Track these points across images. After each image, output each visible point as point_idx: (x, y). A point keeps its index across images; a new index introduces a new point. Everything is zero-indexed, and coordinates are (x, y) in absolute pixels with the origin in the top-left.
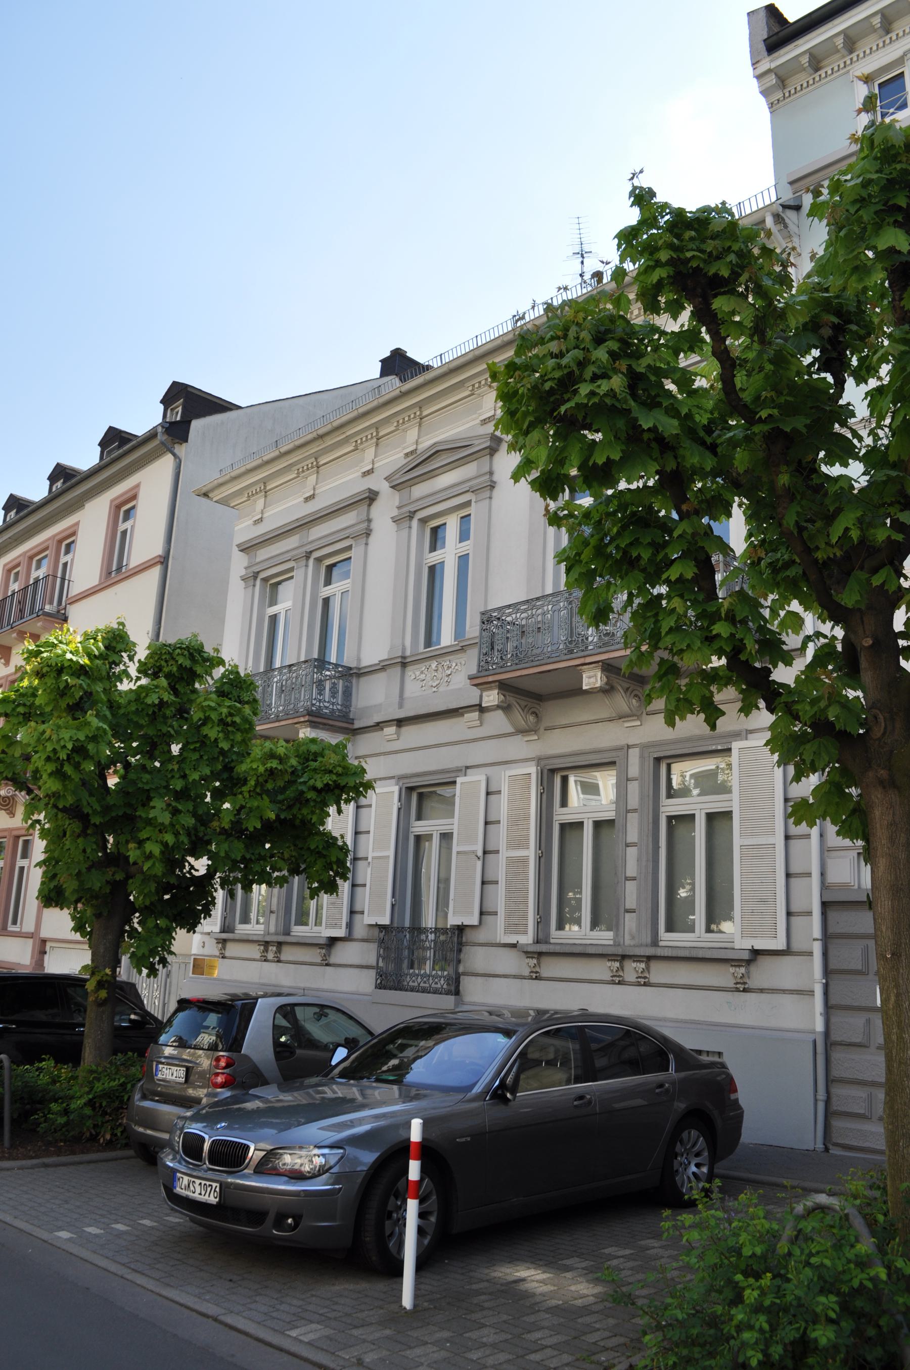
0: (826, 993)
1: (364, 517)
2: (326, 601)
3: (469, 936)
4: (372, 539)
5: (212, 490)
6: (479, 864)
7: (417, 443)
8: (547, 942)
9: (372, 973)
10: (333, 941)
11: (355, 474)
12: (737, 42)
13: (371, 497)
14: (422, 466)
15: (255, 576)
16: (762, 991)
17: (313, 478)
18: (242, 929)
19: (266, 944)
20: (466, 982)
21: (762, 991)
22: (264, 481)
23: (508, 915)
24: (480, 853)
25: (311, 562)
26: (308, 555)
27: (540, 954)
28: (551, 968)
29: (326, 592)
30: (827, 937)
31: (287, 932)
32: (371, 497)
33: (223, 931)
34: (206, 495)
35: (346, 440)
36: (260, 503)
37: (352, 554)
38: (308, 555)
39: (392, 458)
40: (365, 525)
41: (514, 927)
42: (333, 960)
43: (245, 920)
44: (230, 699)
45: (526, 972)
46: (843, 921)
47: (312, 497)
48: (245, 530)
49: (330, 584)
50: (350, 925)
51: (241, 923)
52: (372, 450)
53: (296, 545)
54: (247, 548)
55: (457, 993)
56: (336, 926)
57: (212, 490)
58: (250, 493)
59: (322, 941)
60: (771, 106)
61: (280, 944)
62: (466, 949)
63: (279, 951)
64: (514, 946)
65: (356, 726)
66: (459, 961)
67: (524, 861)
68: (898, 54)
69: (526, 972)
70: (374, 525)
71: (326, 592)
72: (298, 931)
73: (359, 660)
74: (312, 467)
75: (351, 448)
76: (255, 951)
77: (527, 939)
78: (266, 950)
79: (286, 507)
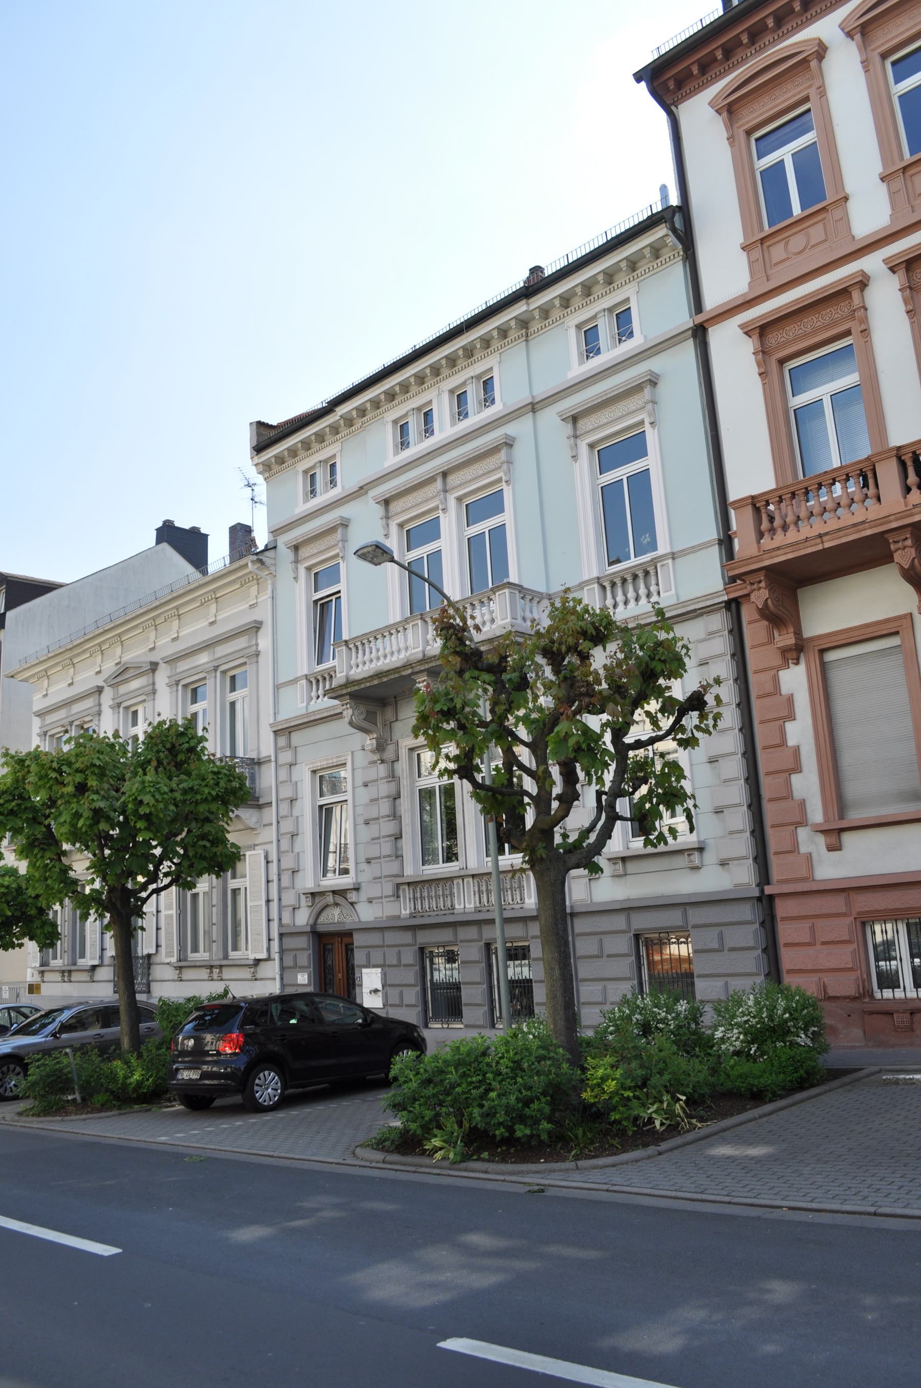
0: (282, 979)
1: (151, 681)
2: (233, 704)
3: (155, 959)
4: (157, 696)
5: (16, 674)
6: (155, 918)
7: (120, 657)
8: (186, 960)
9: (112, 984)
10: (257, 962)
11: (92, 673)
12: (245, 439)
13: (100, 690)
14: (122, 674)
15: (119, 705)
16: (262, 979)
17: (152, 635)
18: (81, 962)
19: (63, 972)
20: (153, 985)
21: (262, 979)
22: (46, 670)
23: (167, 947)
24: (155, 913)
25: (121, 710)
26: (216, 669)
27: (181, 968)
28: (188, 974)
29: (232, 697)
30: (282, 951)
31: (75, 964)
32: (100, 690)
33: (42, 965)
34: (12, 677)
35: (84, 651)
36: (213, 608)
37: (207, 682)
38: (216, 669)
39: (109, 667)
40: (97, 708)
41: (169, 954)
42: (95, 978)
43: (195, 949)
44: (189, 774)
45: (176, 978)
46: (289, 943)
47: (46, 695)
48: (39, 704)
49: (196, 702)
50: (101, 957)
51: (233, 950)
52: (100, 657)
53: (64, 716)
54: (41, 714)
55: (149, 992)
56: (94, 958)
57: (16, 674)
58: (40, 676)
59: (251, 962)
60: (265, 479)
61: (70, 971)
62: (152, 967)
63: (70, 976)
64: (168, 964)
65: (261, 803)
66: (149, 974)
67: (171, 916)
68: (403, 412)
69: (176, 978)
70: (157, 687)
71: (232, 697)
72: (233, 955)
73: (259, 753)
74: (253, 580)
75: (238, 586)
76: (57, 977)
77: (174, 960)
78: (211, 972)
79: (59, 691)
